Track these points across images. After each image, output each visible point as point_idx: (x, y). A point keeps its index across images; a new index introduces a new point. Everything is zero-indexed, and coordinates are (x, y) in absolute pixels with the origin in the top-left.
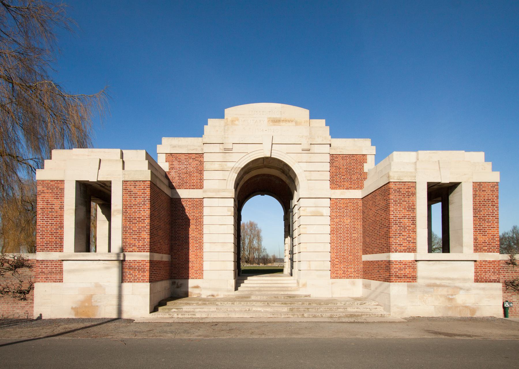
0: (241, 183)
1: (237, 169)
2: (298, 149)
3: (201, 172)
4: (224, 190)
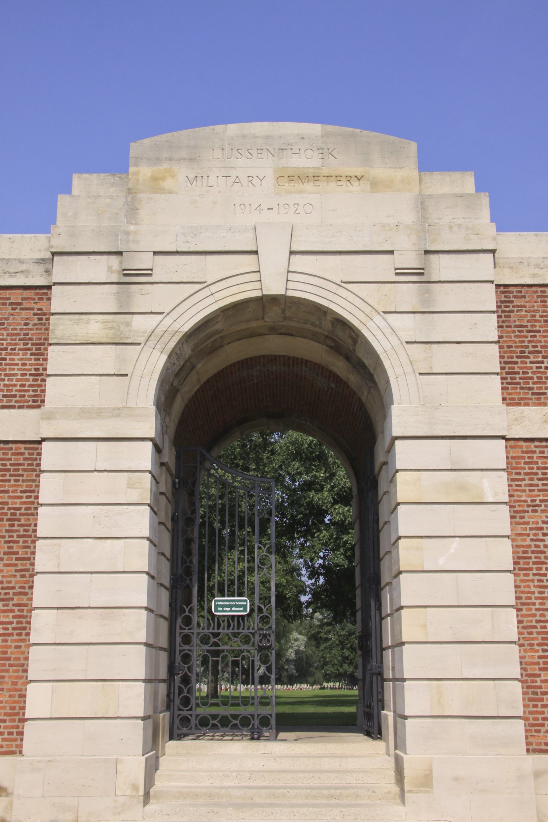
0: (189, 388)
1: (166, 337)
2: (382, 267)
3: (39, 349)
4: (117, 413)
